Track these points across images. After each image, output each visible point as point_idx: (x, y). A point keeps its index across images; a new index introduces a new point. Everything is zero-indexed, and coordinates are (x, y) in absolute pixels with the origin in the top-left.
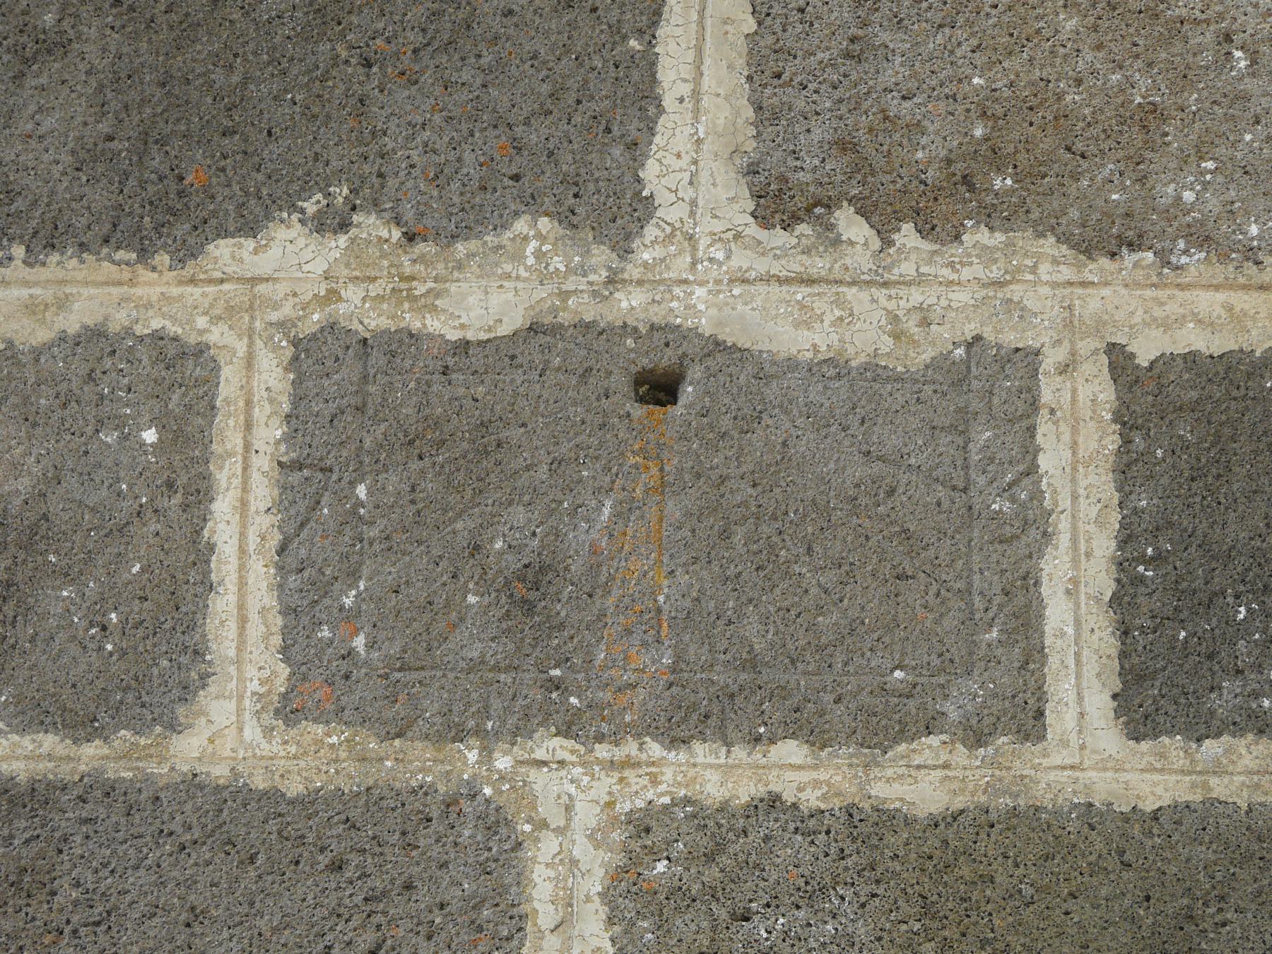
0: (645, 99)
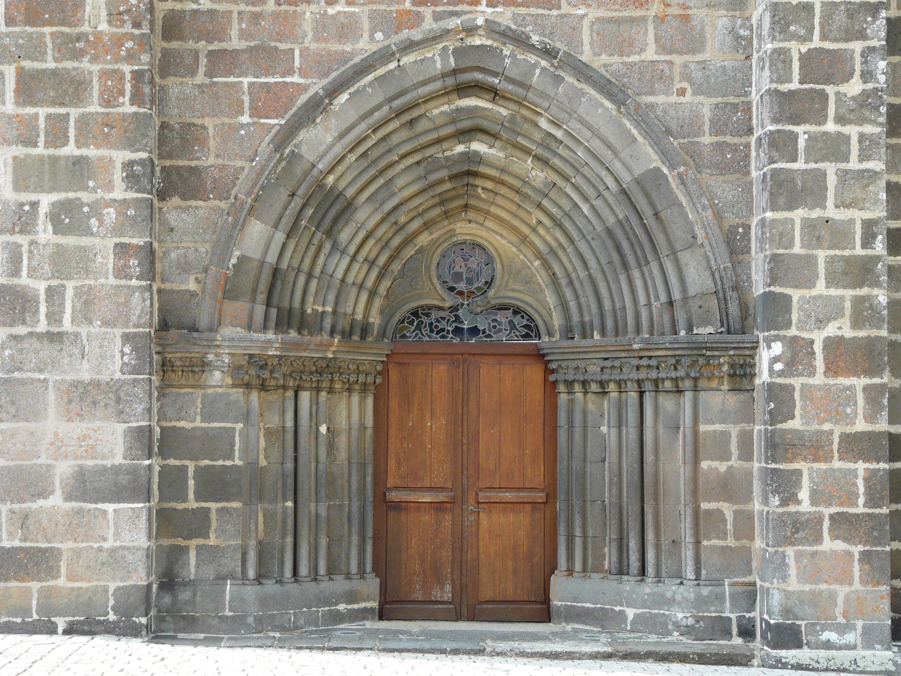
0: (826, 198)
